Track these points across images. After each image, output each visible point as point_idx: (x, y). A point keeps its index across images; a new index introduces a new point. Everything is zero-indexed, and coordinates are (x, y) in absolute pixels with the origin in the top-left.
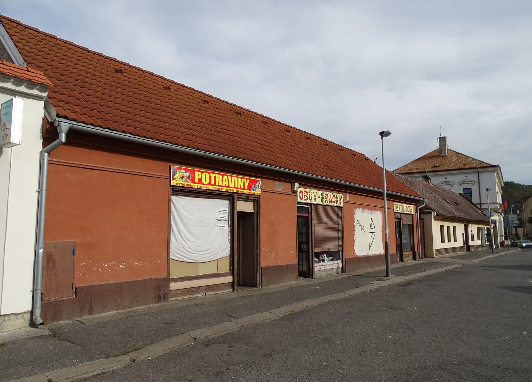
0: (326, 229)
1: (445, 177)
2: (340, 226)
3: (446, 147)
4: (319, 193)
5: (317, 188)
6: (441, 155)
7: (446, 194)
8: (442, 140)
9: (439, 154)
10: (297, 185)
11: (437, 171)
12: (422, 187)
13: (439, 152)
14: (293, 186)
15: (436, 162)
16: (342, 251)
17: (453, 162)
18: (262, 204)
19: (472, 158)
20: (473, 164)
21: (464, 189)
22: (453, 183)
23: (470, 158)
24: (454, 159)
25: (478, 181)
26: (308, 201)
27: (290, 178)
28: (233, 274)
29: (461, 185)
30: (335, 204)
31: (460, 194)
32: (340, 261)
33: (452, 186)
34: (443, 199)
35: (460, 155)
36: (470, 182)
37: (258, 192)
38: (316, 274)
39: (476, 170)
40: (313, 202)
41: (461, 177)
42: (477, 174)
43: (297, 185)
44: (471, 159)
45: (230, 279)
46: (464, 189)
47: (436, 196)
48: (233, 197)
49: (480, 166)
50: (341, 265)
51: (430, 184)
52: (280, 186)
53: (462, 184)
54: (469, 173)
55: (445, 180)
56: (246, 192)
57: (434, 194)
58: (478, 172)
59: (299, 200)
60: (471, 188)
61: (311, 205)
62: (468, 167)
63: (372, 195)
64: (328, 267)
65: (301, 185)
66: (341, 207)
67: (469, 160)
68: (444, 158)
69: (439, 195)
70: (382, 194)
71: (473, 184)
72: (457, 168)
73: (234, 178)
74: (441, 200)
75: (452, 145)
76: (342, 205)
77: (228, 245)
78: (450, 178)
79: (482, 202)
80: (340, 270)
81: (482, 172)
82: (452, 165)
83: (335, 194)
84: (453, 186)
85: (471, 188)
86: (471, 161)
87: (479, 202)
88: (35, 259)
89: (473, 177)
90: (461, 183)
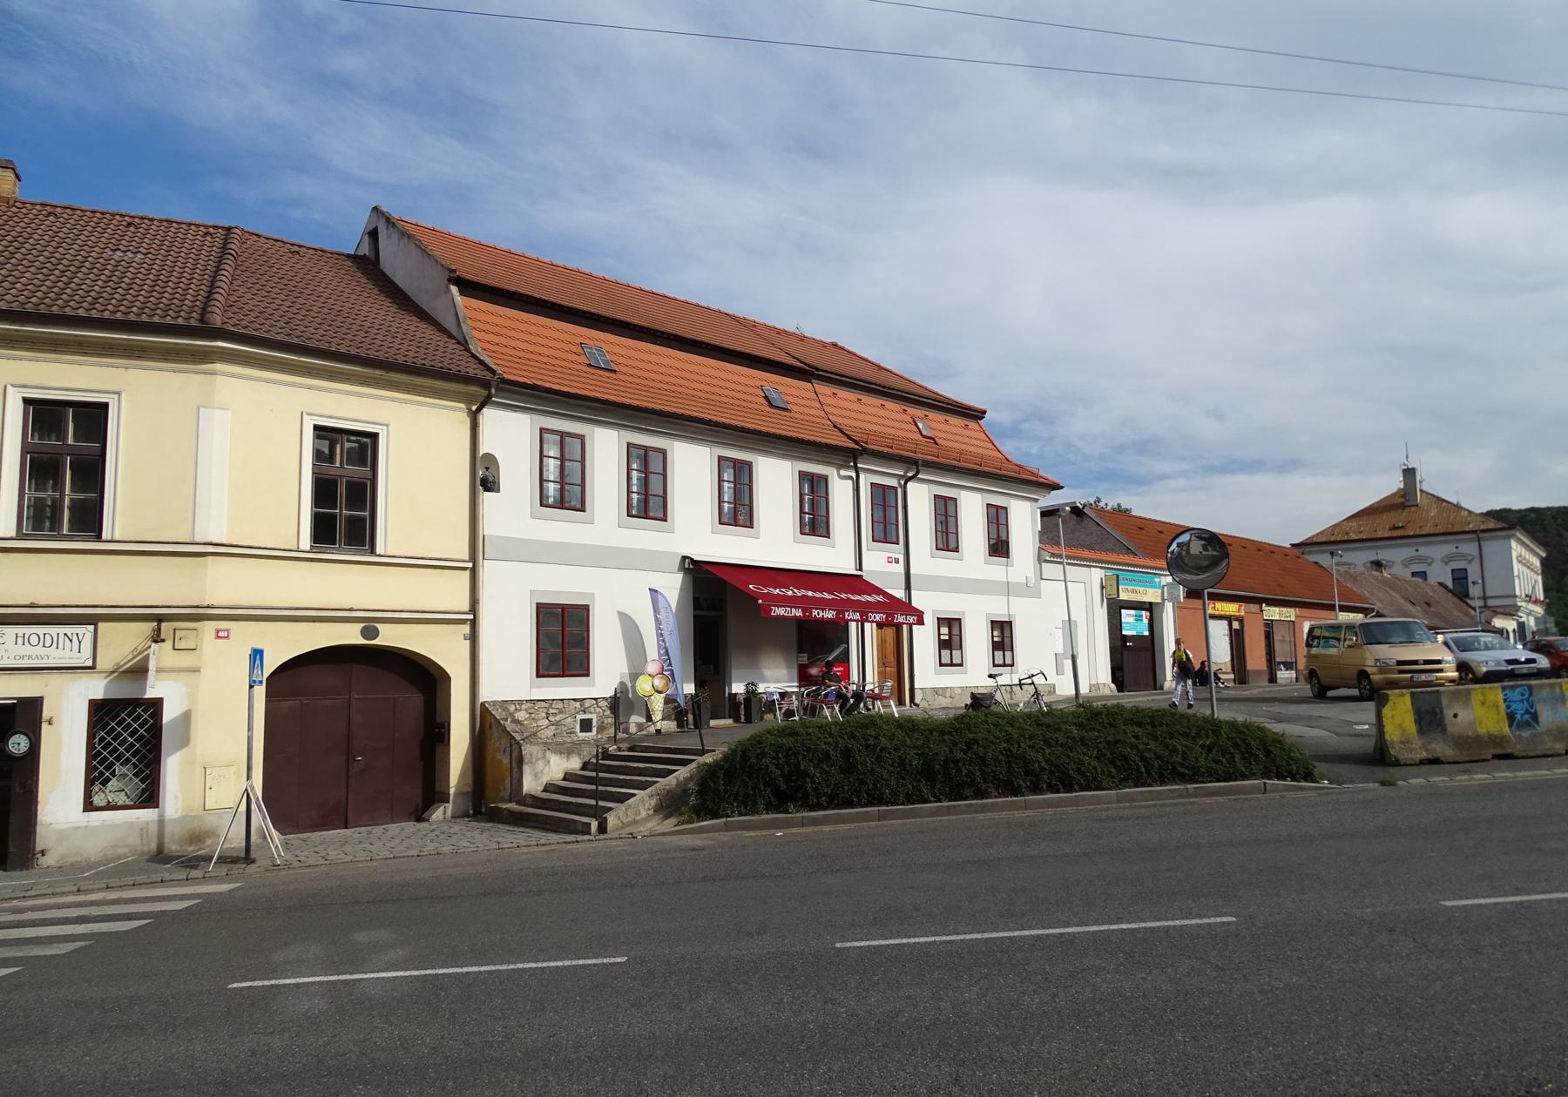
0: (1283, 641)
1: (1415, 548)
2: (1292, 639)
3: (1418, 483)
4: (1277, 609)
5: (1276, 606)
6: (1407, 504)
7: (1410, 589)
8: (1409, 473)
9: (1402, 500)
10: (1264, 605)
11: (1399, 537)
12: (1371, 583)
13: (1402, 496)
14: (1261, 607)
15: (1399, 518)
16: (1296, 662)
17: (1431, 519)
18: (1245, 623)
19: (1469, 512)
20: (1469, 523)
21: (1453, 570)
22: (1430, 560)
23: (1465, 510)
24: (1433, 513)
25: (1478, 556)
26: (1271, 618)
27: (1259, 601)
28: (1234, 673)
29: (1446, 563)
30: (1289, 619)
31: (1441, 584)
32: (1293, 672)
33: (1430, 564)
34: (1405, 599)
35: (1444, 504)
36: (1463, 557)
37: (1242, 614)
38: (1278, 681)
39: (1474, 536)
40: (1273, 618)
41: (1447, 549)
42: (1477, 543)
43: (1264, 605)
44: (1466, 512)
45: (1232, 676)
46: (1453, 570)
47: (1394, 594)
48: (1230, 618)
49: (1482, 527)
50: (1294, 676)
51: (1385, 574)
52: (1254, 608)
53: (1450, 561)
54: (1458, 541)
55: (1416, 554)
56: (1237, 614)
57: (1391, 592)
58: (1479, 540)
59: (1265, 618)
60: (1465, 570)
61: (1271, 620)
62: (1460, 530)
63: (327, 513)
64: (1286, 676)
65: (1268, 605)
66: (1293, 622)
67: (1462, 514)
68: (1413, 509)
69: (1398, 592)
70: (1334, 606)
71: (1470, 562)
72: (1437, 531)
73: (302, 548)
74: (1402, 601)
75: (1431, 482)
76: (1293, 619)
77: (1229, 653)
78: (1426, 551)
79: (1487, 595)
80: (1294, 680)
81: (1487, 539)
82: (1429, 525)
83: (1289, 609)
84: (1433, 565)
85: (1465, 570)
86: (1466, 517)
87: (1482, 595)
88: (53, 894)
89: (1470, 548)
90: (1447, 560)
